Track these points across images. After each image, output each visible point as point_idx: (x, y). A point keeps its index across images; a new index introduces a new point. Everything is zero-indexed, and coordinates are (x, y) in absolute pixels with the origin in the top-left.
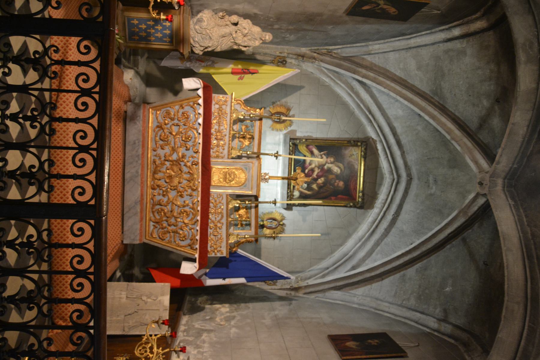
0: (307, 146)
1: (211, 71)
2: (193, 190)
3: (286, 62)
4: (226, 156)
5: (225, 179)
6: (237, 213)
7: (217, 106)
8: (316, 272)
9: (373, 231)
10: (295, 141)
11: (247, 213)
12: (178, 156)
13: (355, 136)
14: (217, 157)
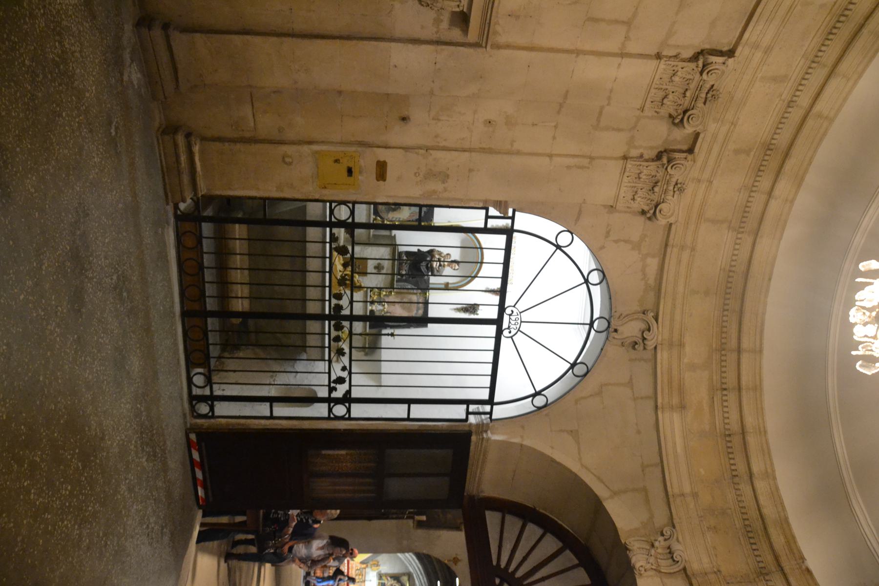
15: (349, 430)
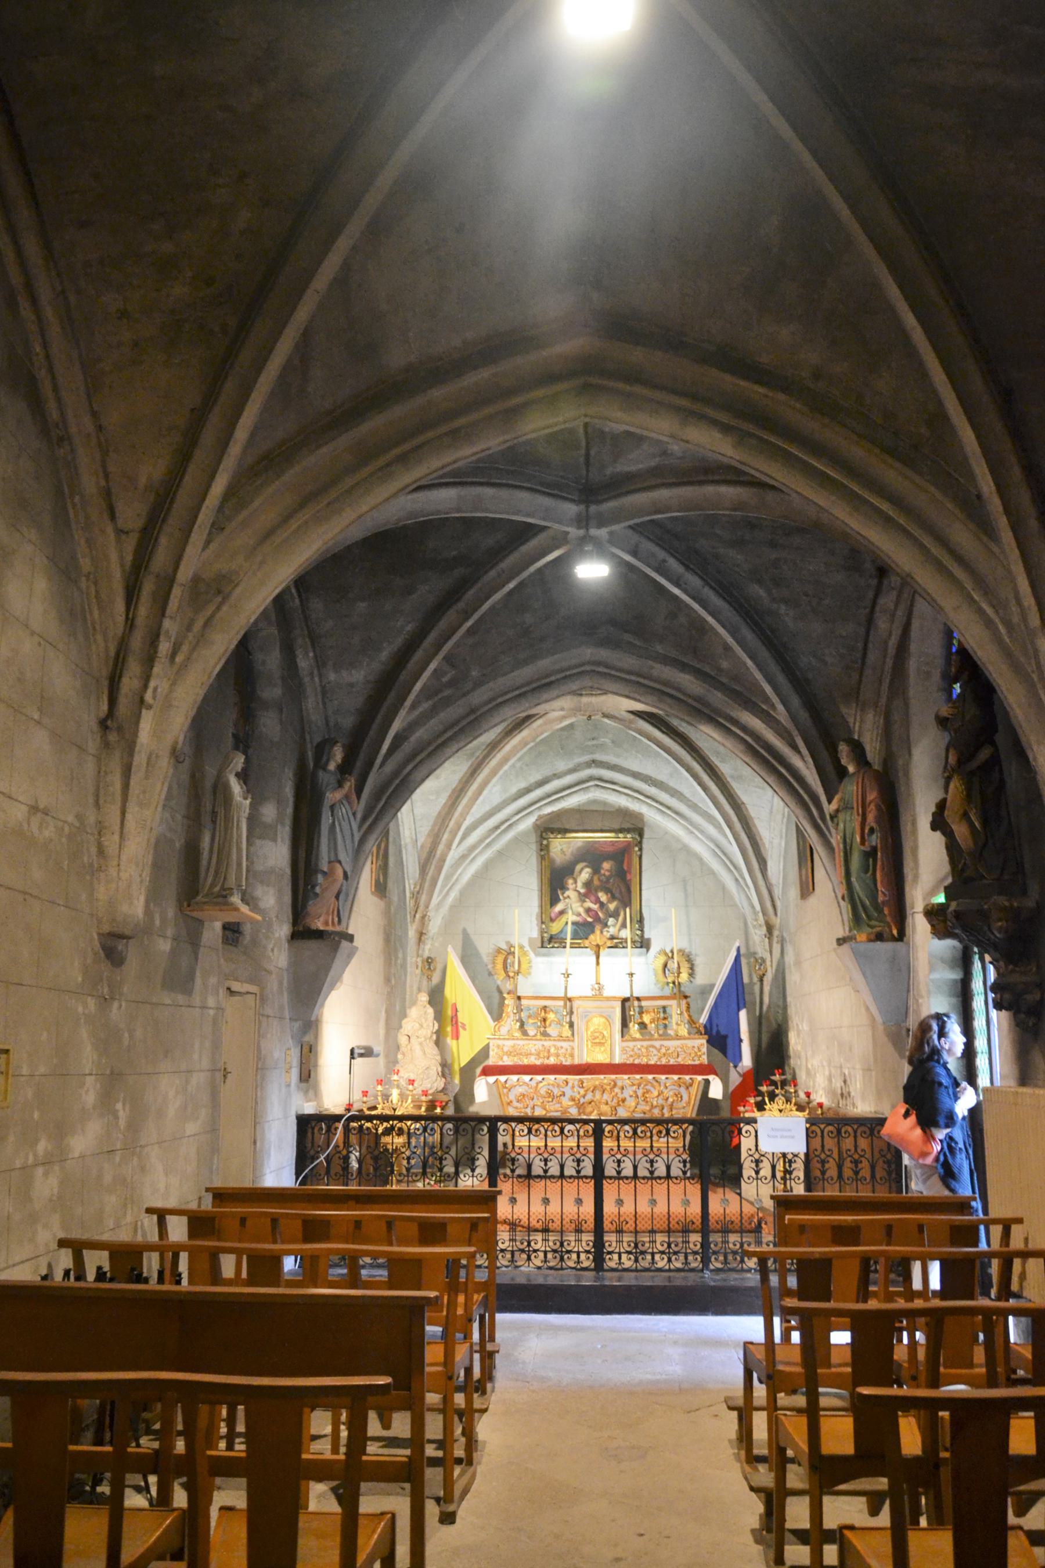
0: (552, 920)
1: (456, 1068)
2: (615, 1085)
3: (429, 958)
4: (571, 1043)
5: (601, 1044)
6: (649, 1026)
7: (505, 1058)
8: (743, 897)
9: (677, 813)
10: (546, 939)
11: (648, 1012)
12: (572, 1106)
13: (534, 847)
14: (572, 1056)
15: (342, 1531)
